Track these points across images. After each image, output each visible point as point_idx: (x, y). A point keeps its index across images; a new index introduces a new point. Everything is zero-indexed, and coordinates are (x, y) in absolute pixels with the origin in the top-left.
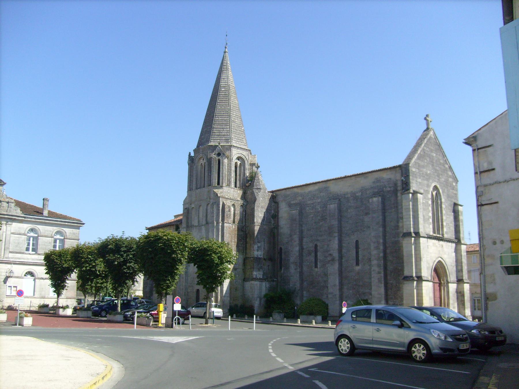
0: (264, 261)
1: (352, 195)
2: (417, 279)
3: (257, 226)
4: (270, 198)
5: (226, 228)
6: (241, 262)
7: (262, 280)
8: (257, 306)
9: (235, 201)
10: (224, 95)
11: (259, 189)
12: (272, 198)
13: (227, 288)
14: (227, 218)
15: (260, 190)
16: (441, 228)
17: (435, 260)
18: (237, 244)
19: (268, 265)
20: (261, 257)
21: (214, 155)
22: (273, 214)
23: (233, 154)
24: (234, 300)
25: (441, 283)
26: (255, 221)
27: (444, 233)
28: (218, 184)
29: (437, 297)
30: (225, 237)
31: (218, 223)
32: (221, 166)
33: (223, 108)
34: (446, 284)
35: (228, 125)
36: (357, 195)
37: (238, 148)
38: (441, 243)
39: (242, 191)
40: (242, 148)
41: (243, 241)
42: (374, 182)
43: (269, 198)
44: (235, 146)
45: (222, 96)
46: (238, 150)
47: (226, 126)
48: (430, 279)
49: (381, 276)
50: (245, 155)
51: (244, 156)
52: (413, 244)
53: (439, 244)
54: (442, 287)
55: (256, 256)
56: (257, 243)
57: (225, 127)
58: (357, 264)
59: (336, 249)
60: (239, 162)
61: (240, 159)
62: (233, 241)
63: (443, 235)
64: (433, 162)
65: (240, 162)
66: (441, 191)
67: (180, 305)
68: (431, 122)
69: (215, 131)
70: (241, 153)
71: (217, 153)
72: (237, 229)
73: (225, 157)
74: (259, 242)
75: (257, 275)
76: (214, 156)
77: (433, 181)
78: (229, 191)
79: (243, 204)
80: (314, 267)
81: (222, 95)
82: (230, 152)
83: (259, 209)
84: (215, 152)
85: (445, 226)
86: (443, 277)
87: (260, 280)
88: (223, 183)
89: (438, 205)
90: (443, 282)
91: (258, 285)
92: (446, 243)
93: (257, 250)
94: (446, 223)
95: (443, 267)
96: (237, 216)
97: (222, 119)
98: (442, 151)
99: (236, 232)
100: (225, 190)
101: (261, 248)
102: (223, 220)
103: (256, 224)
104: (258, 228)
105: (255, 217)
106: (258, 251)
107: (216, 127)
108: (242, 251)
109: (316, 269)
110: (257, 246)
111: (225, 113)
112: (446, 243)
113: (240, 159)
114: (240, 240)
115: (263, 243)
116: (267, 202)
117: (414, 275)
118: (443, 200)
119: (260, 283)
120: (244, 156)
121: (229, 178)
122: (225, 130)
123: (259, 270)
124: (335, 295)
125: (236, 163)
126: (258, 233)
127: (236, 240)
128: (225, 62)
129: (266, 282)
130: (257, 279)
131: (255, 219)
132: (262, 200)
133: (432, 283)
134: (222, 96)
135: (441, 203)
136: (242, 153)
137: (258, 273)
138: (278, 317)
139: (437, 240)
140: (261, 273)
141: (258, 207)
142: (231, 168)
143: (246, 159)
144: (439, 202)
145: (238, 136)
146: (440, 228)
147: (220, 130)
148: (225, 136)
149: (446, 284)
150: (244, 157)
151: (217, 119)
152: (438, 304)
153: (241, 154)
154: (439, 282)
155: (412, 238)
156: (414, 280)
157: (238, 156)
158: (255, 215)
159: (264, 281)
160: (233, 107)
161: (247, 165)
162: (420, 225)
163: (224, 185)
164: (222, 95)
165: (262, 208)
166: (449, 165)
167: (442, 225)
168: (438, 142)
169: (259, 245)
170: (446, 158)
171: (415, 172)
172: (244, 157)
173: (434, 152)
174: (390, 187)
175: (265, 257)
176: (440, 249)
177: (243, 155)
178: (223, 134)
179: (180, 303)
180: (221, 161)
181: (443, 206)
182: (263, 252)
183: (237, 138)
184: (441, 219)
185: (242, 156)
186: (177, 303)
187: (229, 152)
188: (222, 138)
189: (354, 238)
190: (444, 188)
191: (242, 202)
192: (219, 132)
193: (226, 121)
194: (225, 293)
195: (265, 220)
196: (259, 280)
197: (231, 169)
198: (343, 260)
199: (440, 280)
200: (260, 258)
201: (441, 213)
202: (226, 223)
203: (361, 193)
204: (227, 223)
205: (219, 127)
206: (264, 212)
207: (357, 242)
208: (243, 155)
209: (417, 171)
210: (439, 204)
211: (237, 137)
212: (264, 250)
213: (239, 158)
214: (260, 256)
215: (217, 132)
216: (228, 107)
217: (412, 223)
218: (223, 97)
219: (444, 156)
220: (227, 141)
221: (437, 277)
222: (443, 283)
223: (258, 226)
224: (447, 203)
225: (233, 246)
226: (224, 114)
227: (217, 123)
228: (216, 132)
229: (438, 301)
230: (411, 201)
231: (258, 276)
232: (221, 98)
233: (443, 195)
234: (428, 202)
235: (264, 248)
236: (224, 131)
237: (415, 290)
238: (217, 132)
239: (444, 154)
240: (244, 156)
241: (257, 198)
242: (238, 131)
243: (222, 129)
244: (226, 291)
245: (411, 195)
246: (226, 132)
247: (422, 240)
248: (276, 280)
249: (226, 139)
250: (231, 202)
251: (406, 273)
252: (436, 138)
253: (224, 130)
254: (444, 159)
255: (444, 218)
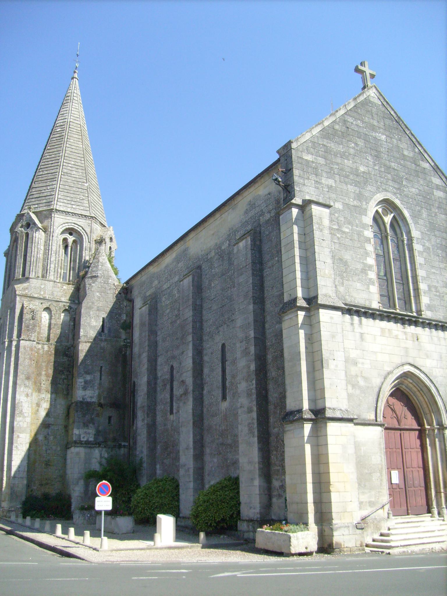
0: (99, 408)
1: (216, 251)
2: (313, 417)
3: (85, 344)
4: (119, 293)
5: (25, 349)
6: (62, 412)
7: (93, 444)
8: (78, 496)
9: (50, 303)
10: (59, 137)
11: (95, 277)
12: (123, 292)
13: (22, 461)
14: (28, 330)
15: (95, 279)
16: (415, 297)
17: (389, 369)
18: (53, 378)
19: (110, 418)
20: (93, 400)
21: (22, 227)
22: (125, 321)
23: (56, 224)
24: (41, 485)
25: (425, 430)
26: (82, 334)
27: (423, 308)
28: (24, 275)
29: (415, 464)
30: (21, 365)
31: (10, 342)
32: (29, 245)
33: (53, 156)
34: (436, 431)
35: (55, 179)
36: (223, 248)
37: (67, 213)
38: (412, 329)
39: (74, 286)
40: (75, 214)
41: (68, 373)
42: (246, 212)
43: (117, 292)
44: (59, 211)
45: (55, 139)
46: (68, 218)
47: (52, 182)
48: (373, 417)
49: (253, 419)
50: (82, 226)
51: (79, 227)
52: (300, 325)
53: (405, 333)
54: (428, 440)
55: (81, 400)
56: (83, 375)
57: (51, 184)
58: (224, 398)
59: (189, 369)
60: (71, 239)
61: (74, 234)
62: (44, 373)
63: (419, 312)
64: (379, 152)
65: (74, 238)
66: (406, 213)
67: (110, 499)
68: (372, 76)
69: (34, 191)
70: (74, 222)
71: (24, 223)
72: (53, 352)
73: (36, 228)
74: (88, 373)
75: (82, 436)
76: (20, 229)
77: (378, 188)
78: (43, 286)
79: (69, 307)
80: (169, 414)
81: (55, 137)
82: (50, 221)
83: (91, 313)
84: (22, 222)
85: (425, 293)
86: (429, 416)
87: (88, 444)
88: (30, 273)
89: (403, 245)
90: (429, 427)
91: (82, 455)
92: (431, 332)
93: (82, 388)
94: (429, 287)
95: (425, 389)
96: (55, 329)
97: (49, 172)
98: (408, 132)
99: (52, 359)
100: (33, 285)
101: (93, 384)
102: (19, 335)
103: (82, 339)
104: (86, 346)
105: (81, 327)
106: (85, 388)
107: (37, 186)
108: (65, 393)
109: (172, 416)
110: (83, 380)
111: (55, 163)
112: (431, 332)
113: (74, 234)
114: (61, 371)
115: (98, 374)
116: (112, 299)
117: (306, 406)
118: (415, 233)
119: (88, 450)
120: (81, 227)
121: (46, 265)
122: (49, 188)
123: (86, 425)
124: (189, 468)
125: (65, 240)
126: (86, 356)
127: (51, 372)
128: (70, 91)
129: (100, 449)
130: (78, 443)
131: (81, 330)
132: (99, 298)
133: (379, 430)
134: (55, 139)
135: (410, 239)
136: (76, 222)
137: (82, 431)
138: (79, 517)
139: (396, 322)
140: (92, 431)
141: (90, 308)
142: (50, 247)
143: (84, 232)
144: (405, 237)
145: (72, 196)
146: (412, 298)
147: (41, 189)
148: (47, 198)
149: (436, 431)
150: (81, 228)
151: (41, 173)
152: (416, 482)
153: (74, 223)
154: (419, 428)
155: (297, 311)
156: (301, 420)
157: (67, 227)
158: (82, 322)
159: (96, 447)
160: (69, 153)
161: (87, 241)
162: (319, 278)
163: (32, 275)
164: (55, 137)
165: (98, 310)
166: (433, 164)
167: (417, 289)
168: (392, 113)
169: (88, 378)
170: (420, 148)
171: (313, 162)
172: (79, 229)
173: (381, 130)
174: (269, 212)
175: (102, 401)
176: (410, 344)
177: (77, 225)
178: (45, 194)
179: (109, 496)
180: (30, 236)
181: (417, 247)
182: (97, 392)
183: (68, 198)
184: (412, 277)
185: (76, 227)
186: (104, 494)
187: (47, 220)
188: (42, 202)
189: (219, 340)
190: (418, 208)
191: (68, 304)
192: (39, 192)
193: (53, 174)
194: (16, 472)
195: (106, 331)
196: (84, 445)
197: (50, 249)
198: (205, 392)
199: (420, 423)
200: (88, 404)
201: (411, 263)
202: (23, 340)
203: (228, 242)
204: (27, 340)
205: (40, 185)
206: (103, 318)
207: (223, 346)
208: (77, 225)
209: (321, 161)
210: (405, 242)
211: (69, 198)
212: (99, 388)
213: (72, 232)
214: (89, 400)
215: (37, 192)
216: (61, 154)
217: (298, 274)
218: (57, 140)
219: (415, 142)
220: (49, 203)
221: (413, 415)
222: (429, 429)
223: (86, 342)
224: (429, 240)
225: (44, 382)
226: (52, 165)
227: (40, 179)
228: (35, 193)
229: (416, 474)
230: (296, 225)
231: (84, 437)
232: (54, 142)
233: (416, 223)
234: (362, 232)
235: (100, 384)
236: (47, 191)
237: (308, 448)
238: (37, 192)
239: (414, 140)
240: (81, 227)
241: (87, 292)
242: (74, 189)
243: (44, 188)
244: (19, 467)
245: (295, 211)
246: (50, 190)
247: (324, 315)
248: (127, 444)
249: (49, 201)
250: (42, 303)
251: (290, 405)
252: (386, 103)
253: (47, 189)
254: (417, 150)
255: (421, 273)
